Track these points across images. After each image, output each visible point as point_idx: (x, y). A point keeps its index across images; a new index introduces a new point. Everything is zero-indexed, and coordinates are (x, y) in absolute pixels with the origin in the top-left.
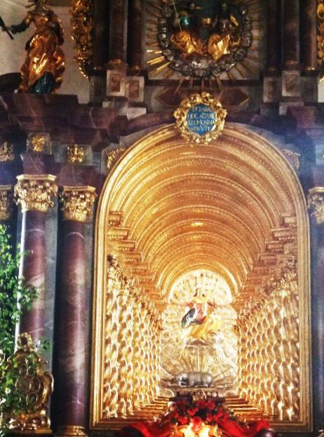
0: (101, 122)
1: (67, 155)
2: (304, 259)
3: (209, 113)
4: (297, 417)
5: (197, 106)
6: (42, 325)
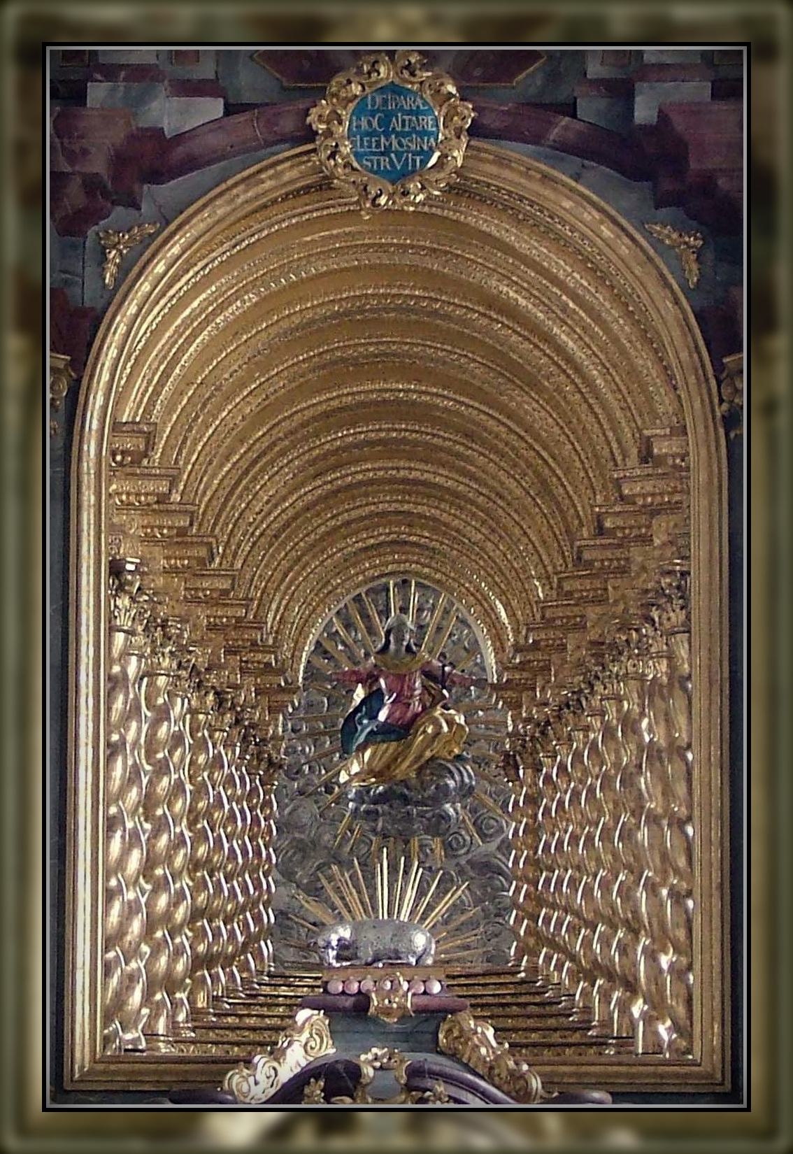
0: (85, 152)
2: (711, 568)
3: (417, 113)
4: (683, 1044)
5: (382, 90)
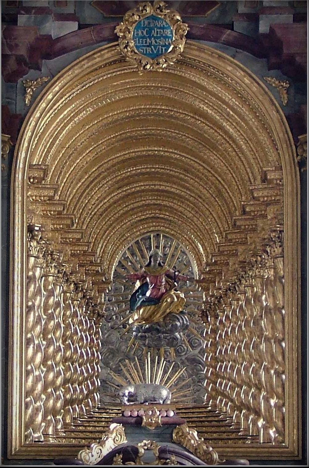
0: (17, 45)
2: (293, 229)
3: (163, 28)
4: (281, 438)
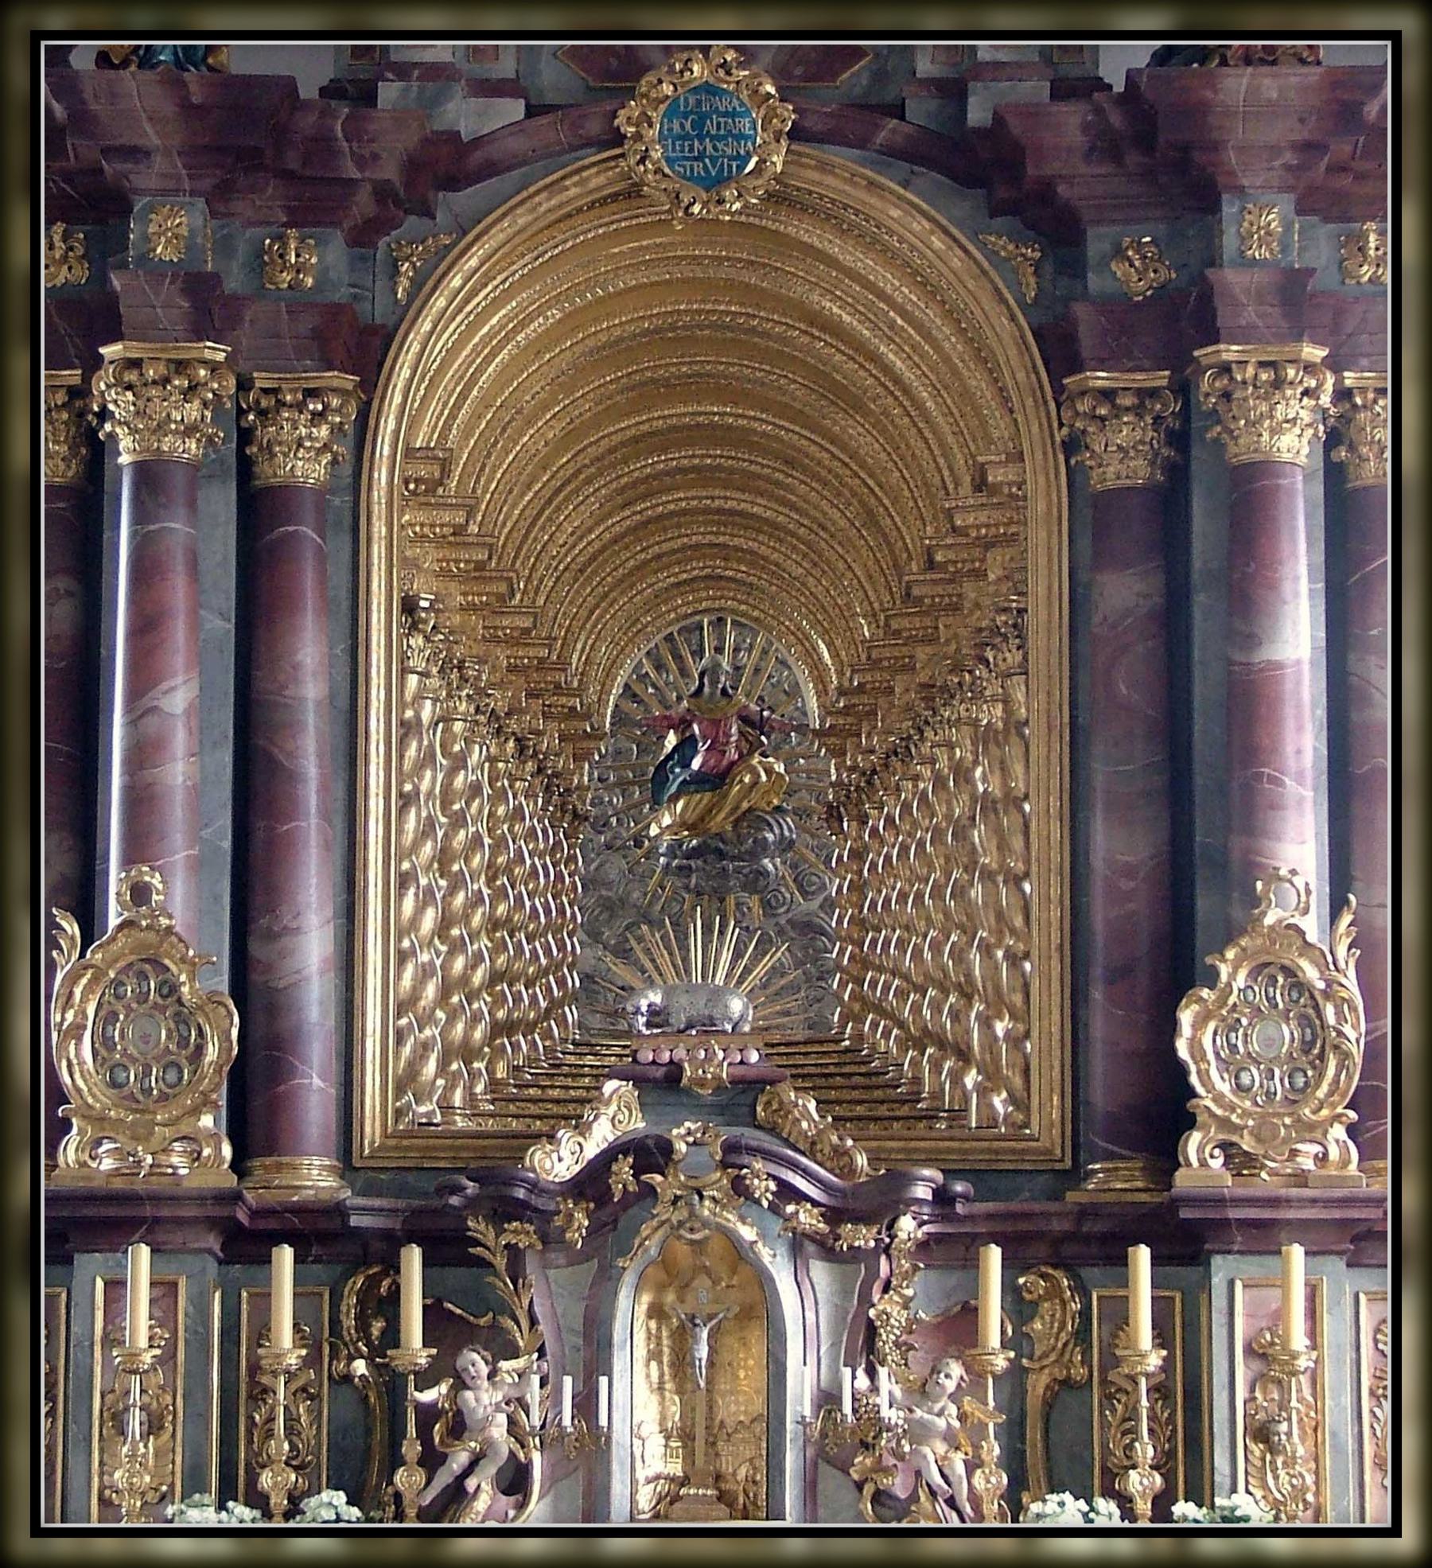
1: (259, 263)
2: (1050, 605)
6: (194, 838)
